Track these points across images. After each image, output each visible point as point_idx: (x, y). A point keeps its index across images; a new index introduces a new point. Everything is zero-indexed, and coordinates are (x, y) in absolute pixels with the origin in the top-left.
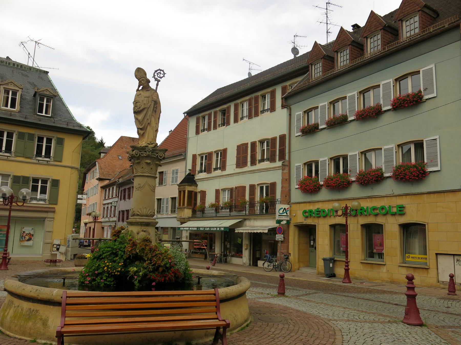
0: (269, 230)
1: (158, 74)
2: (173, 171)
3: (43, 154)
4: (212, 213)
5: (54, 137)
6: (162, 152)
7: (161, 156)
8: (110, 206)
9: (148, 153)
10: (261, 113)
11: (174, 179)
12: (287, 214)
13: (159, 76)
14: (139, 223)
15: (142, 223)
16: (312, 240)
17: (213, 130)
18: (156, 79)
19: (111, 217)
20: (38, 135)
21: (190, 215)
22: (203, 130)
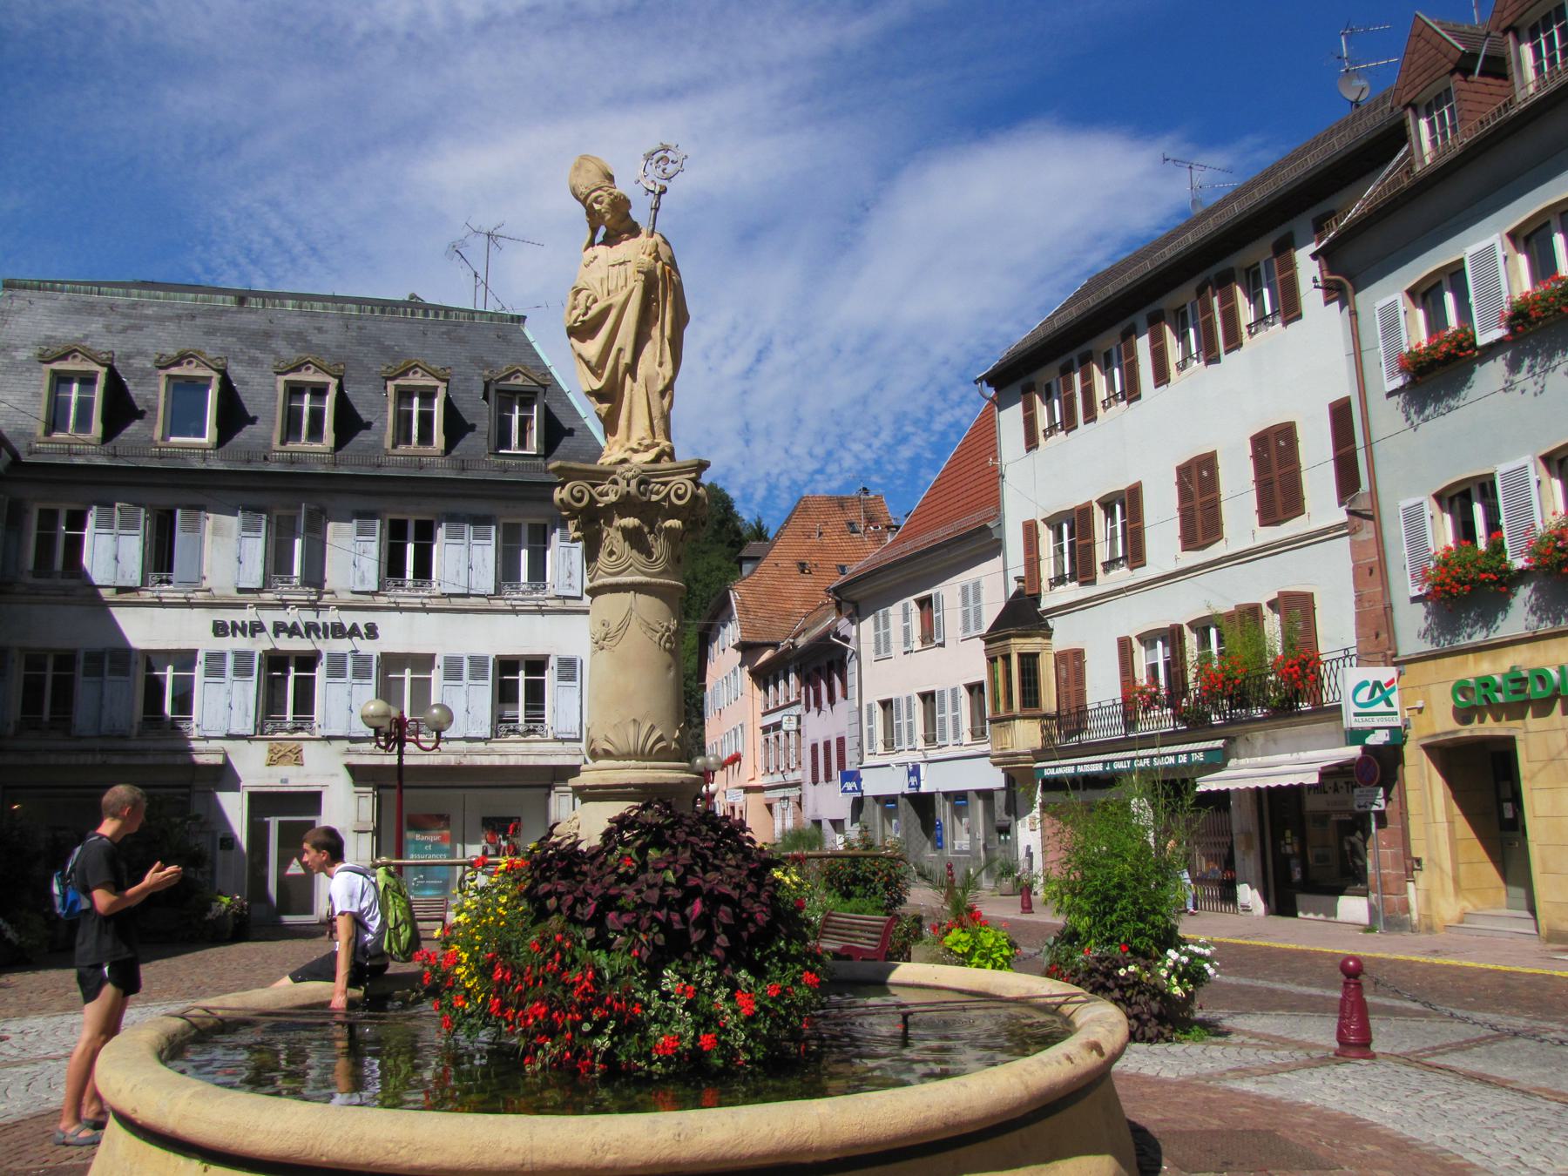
0: (1325, 774)
2: (965, 589)
4: (1111, 727)
7: (680, 492)
10: (1250, 332)
11: (970, 618)
12: (1389, 704)
16: (1508, 800)
17: (1086, 423)
22: (1051, 430)
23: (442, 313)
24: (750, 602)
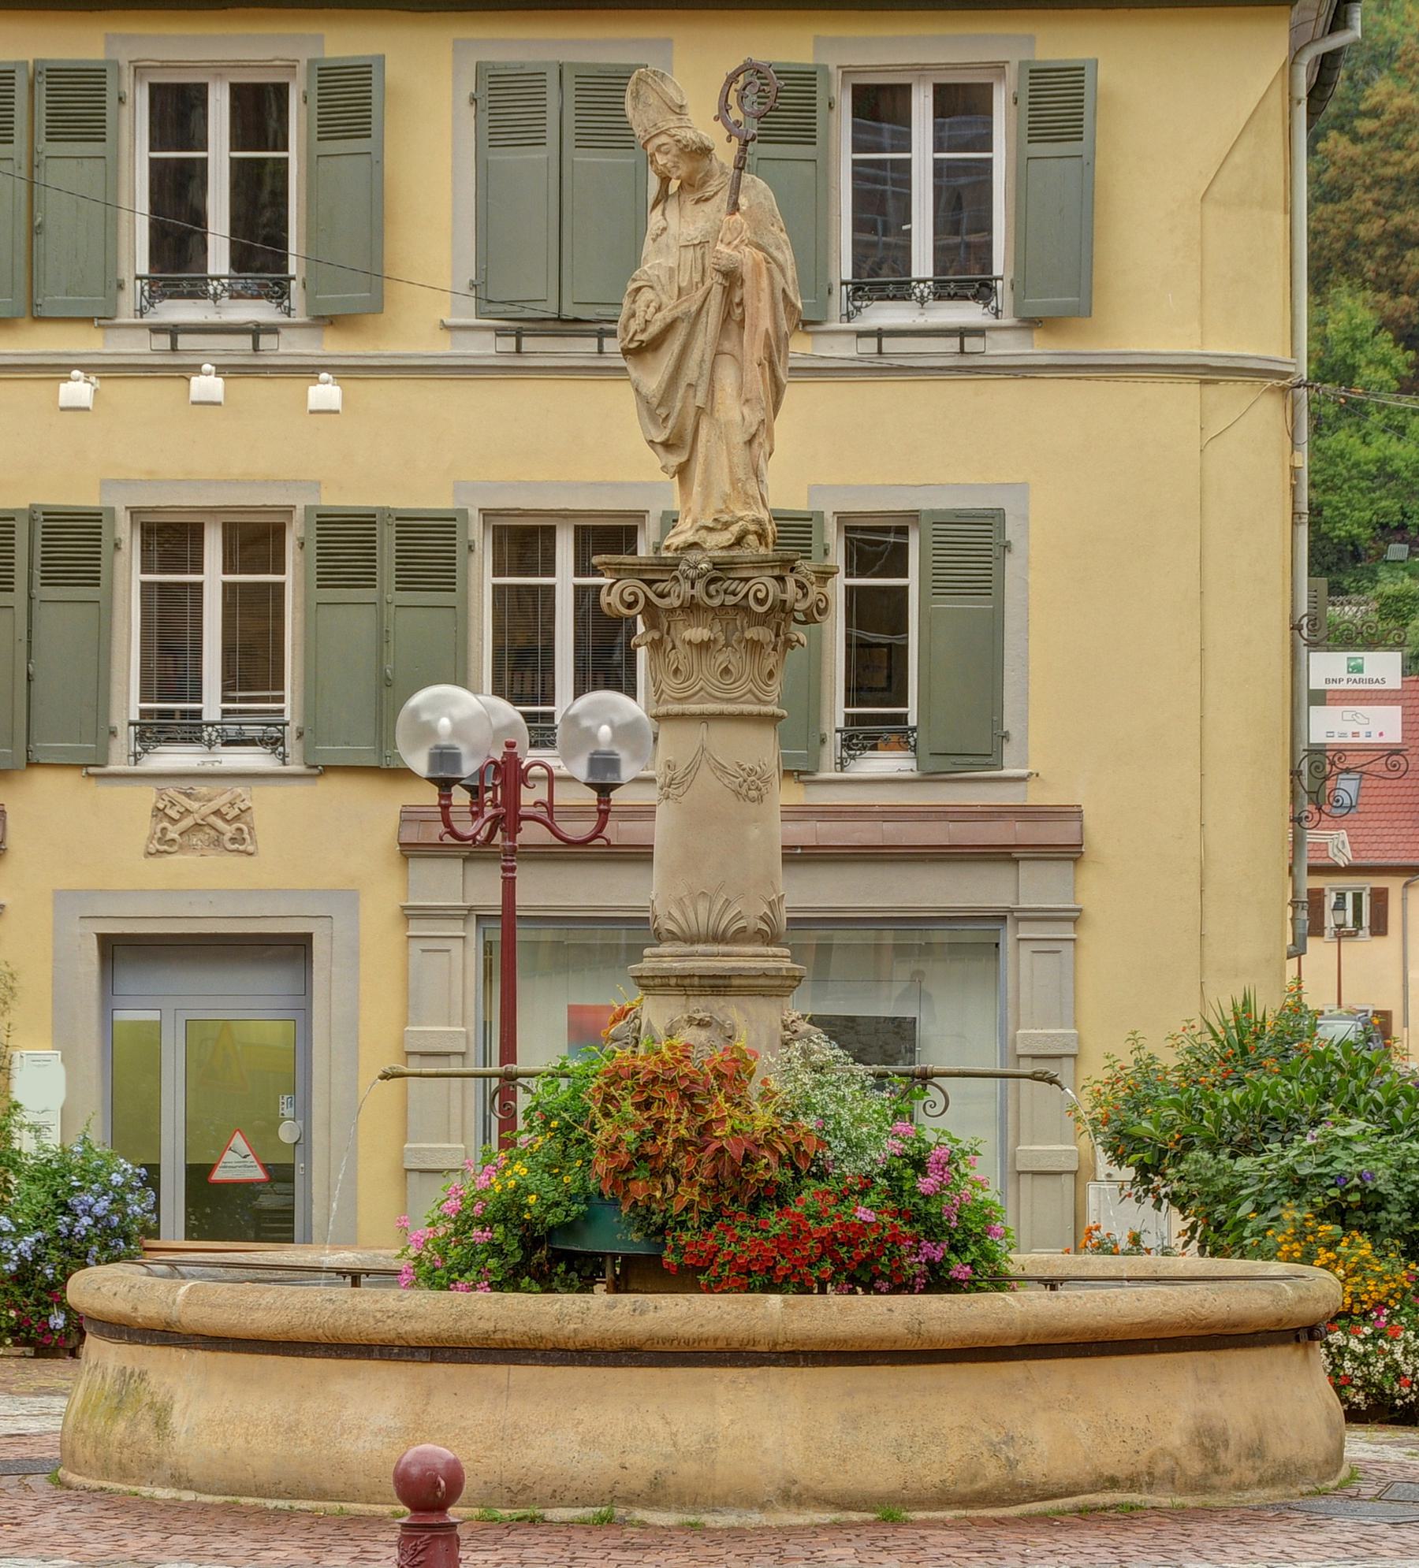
3: (922, 263)
5: (999, 67)
6: (769, 572)
7: (761, 595)
9: (686, 586)
14: (673, 981)
15: (687, 982)
20: (847, 71)
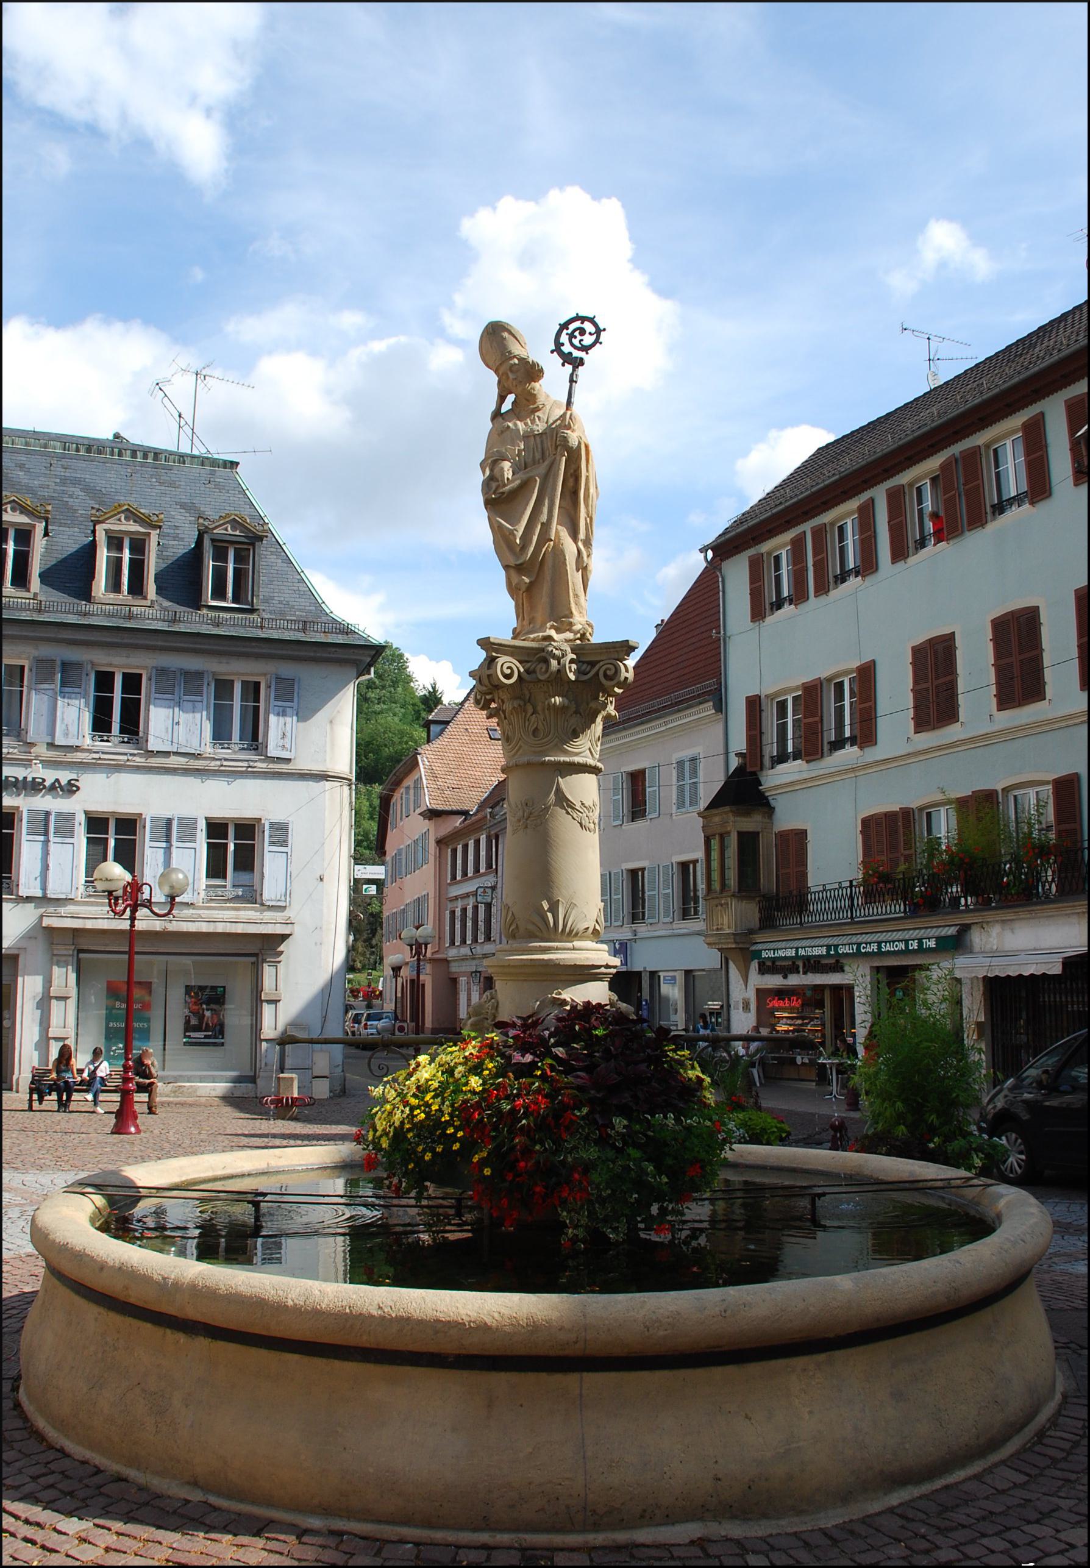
1: (571, 336)
4: (836, 910)
7: (609, 673)
8: (471, 901)
11: (686, 796)
13: (576, 342)
17: (815, 596)
18: (567, 359)
19: (476, 941)
21: (755, 923)
23: (151, 455)
24: (438, 768)
